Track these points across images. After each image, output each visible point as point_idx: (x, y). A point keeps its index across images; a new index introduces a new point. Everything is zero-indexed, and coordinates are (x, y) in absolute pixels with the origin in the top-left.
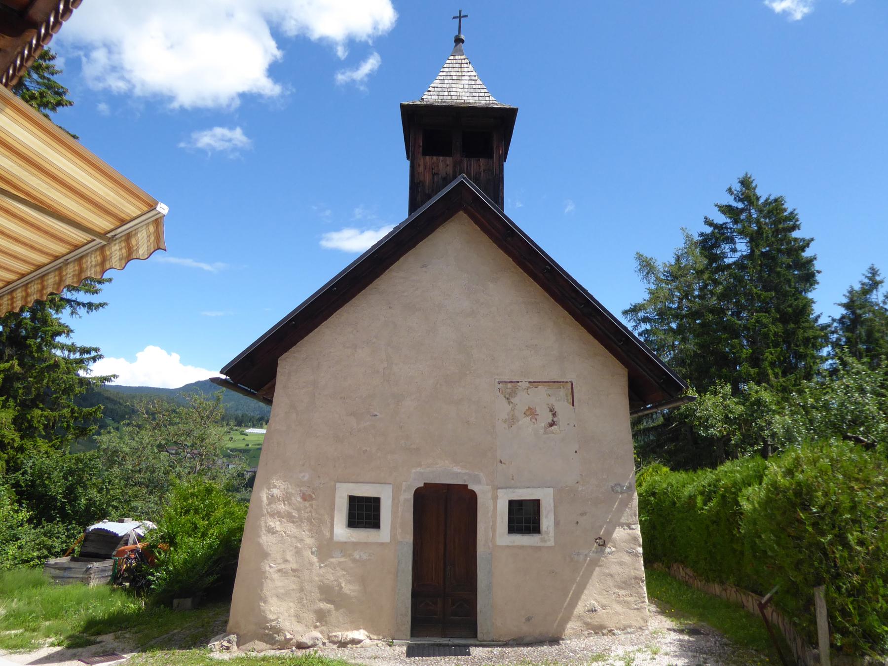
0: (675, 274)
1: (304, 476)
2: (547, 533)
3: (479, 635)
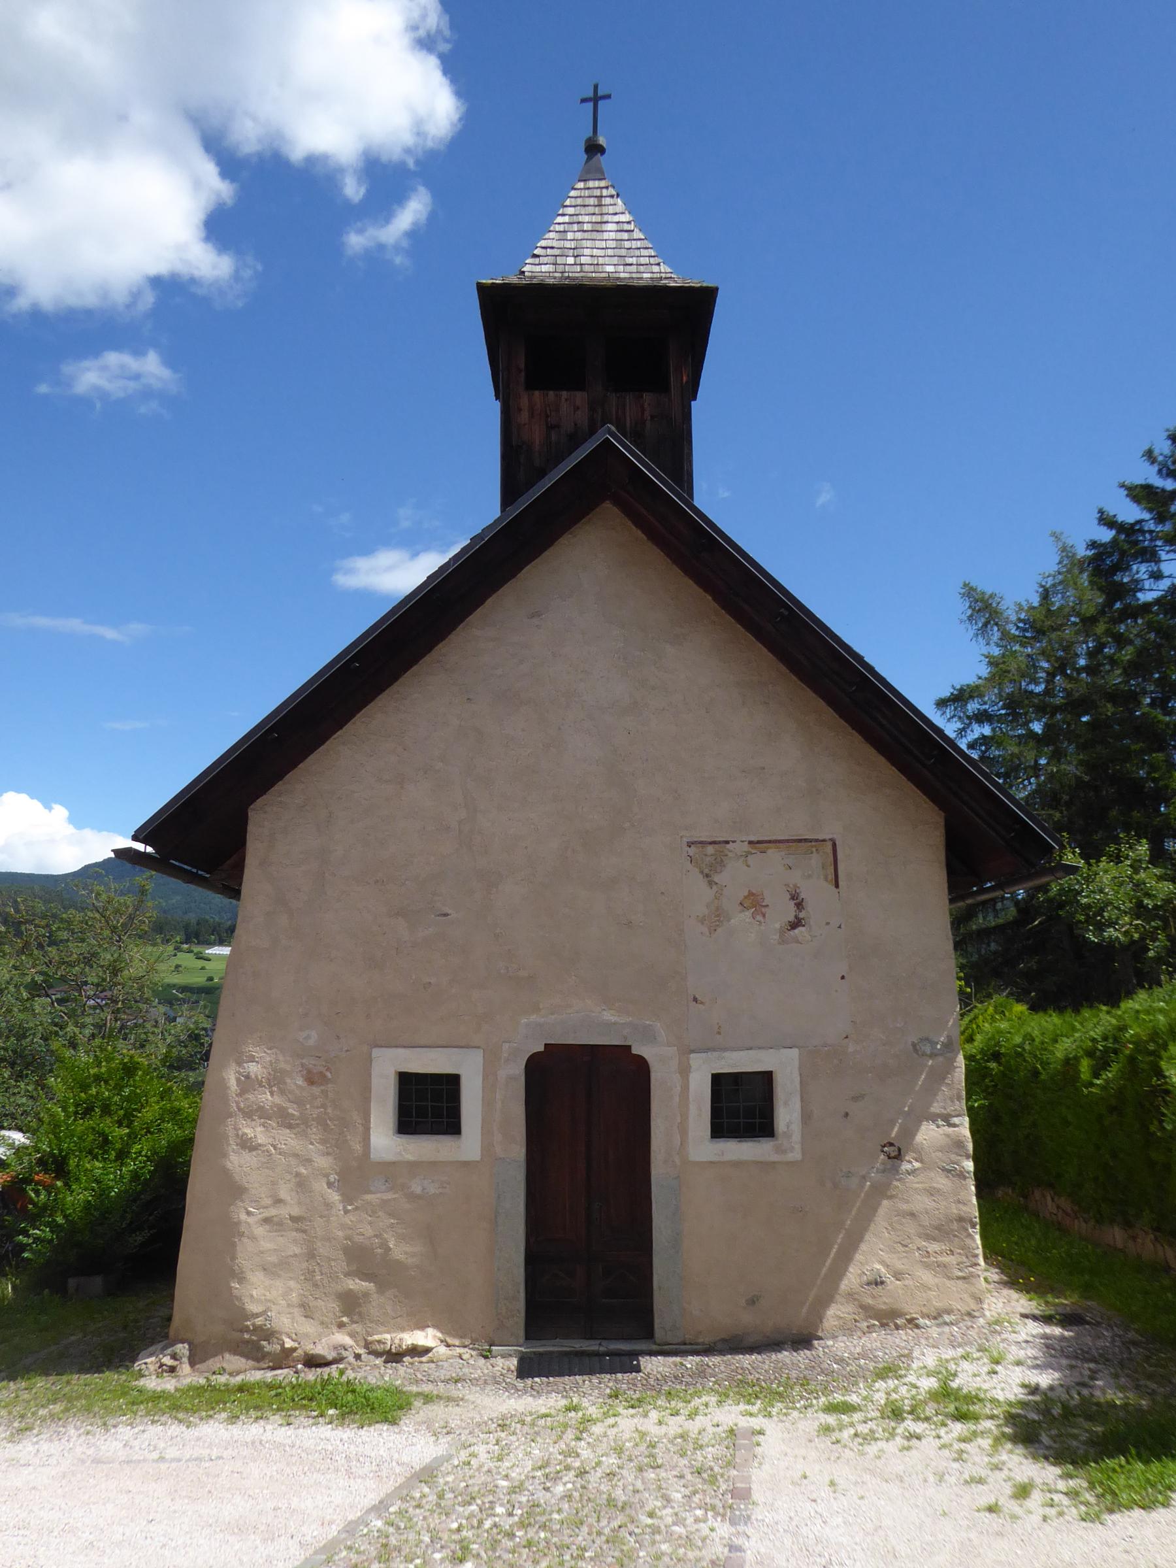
0: (1041, 625)
1: (308, 1037)
2: (788, 1135)
3: (659, 1333)
